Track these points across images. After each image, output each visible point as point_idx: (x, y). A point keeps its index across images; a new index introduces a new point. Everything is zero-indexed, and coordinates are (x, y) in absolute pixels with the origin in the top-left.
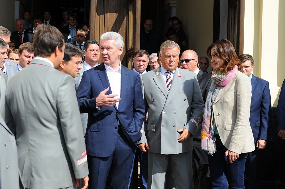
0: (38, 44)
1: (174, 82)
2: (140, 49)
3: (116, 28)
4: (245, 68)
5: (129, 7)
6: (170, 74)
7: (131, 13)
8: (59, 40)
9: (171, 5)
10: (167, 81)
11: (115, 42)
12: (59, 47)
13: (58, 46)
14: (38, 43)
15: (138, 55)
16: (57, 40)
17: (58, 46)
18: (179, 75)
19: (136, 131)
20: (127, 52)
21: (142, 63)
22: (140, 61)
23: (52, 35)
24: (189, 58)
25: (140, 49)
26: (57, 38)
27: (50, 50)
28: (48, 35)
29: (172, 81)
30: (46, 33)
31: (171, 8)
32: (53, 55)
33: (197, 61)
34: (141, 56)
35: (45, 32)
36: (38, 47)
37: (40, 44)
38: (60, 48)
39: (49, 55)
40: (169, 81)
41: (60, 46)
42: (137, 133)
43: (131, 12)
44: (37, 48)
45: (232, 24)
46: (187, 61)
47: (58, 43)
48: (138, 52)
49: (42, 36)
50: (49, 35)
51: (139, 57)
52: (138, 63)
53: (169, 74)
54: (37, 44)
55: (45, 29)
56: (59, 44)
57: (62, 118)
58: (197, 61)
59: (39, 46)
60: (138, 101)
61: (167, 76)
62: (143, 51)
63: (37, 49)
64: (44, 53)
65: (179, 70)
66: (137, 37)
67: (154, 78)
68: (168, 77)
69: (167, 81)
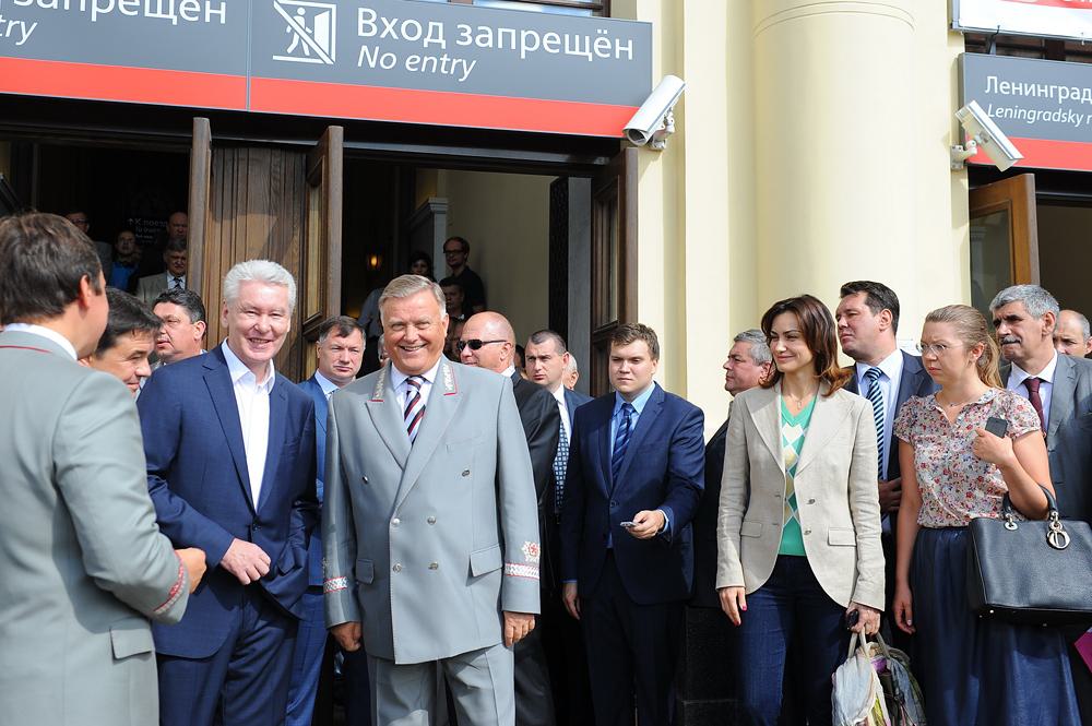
0: (15, 282)
1: (429, 414)
2: (342, 314)
3: (274, 253)
4: (631, 365)
5: (309, 195)
6: (419, 387)
7: (314, 216)
8: (84, 254)
9: (433, 208)
10: (407, 413)
11: (265, 288)
12: (88, 280)
13: (84, 277)
14: (14, 279)
15: (334, 331)
16: (78, 259)
17: (84, 277)
18: (450, 388)
19: (297, 567)
20: (304, 328)
21: (347, 356)
22: (340, 348)
23: (58, 245)
24: (482, 339)
25: (342, 314)
26: (77, 251)
27: (61, 294)
28: (44, 248)
29: (424, 407)
30: (37, 244)
31: (432, 215)
32: (72, 310)
33: (508, 346)
34: (344, 334)
35: (29, 241)
36: (17, 291)
37: (20, 282)
38: (94, 281)
39: (57, 311)
40: (416, 409)
41: (90, 274)
42: (301, 570)
43: (317, 212)
44: (11, 296)
45: (605, 261)
46: (476, 344)
47: (82, 266)
48: (334, 323)
49: (23, 256)
50: (48, 246)
51: (338, 336)
52: (337, 354)
53: (414, 390)
54: (12, 282)
55: (27, 231)
56: (86, 271)
57: (128, 413)
58: (508, 346)
59: (19, 288)
60: (315, 488)
61: (408, 392)
62: (348, 319)
63: (12, 299)
64: (40, 309)
65: (453, 372)
66: (330, 282)
67: (370, 404)
68: (413, 395)
69: (407, 413)
